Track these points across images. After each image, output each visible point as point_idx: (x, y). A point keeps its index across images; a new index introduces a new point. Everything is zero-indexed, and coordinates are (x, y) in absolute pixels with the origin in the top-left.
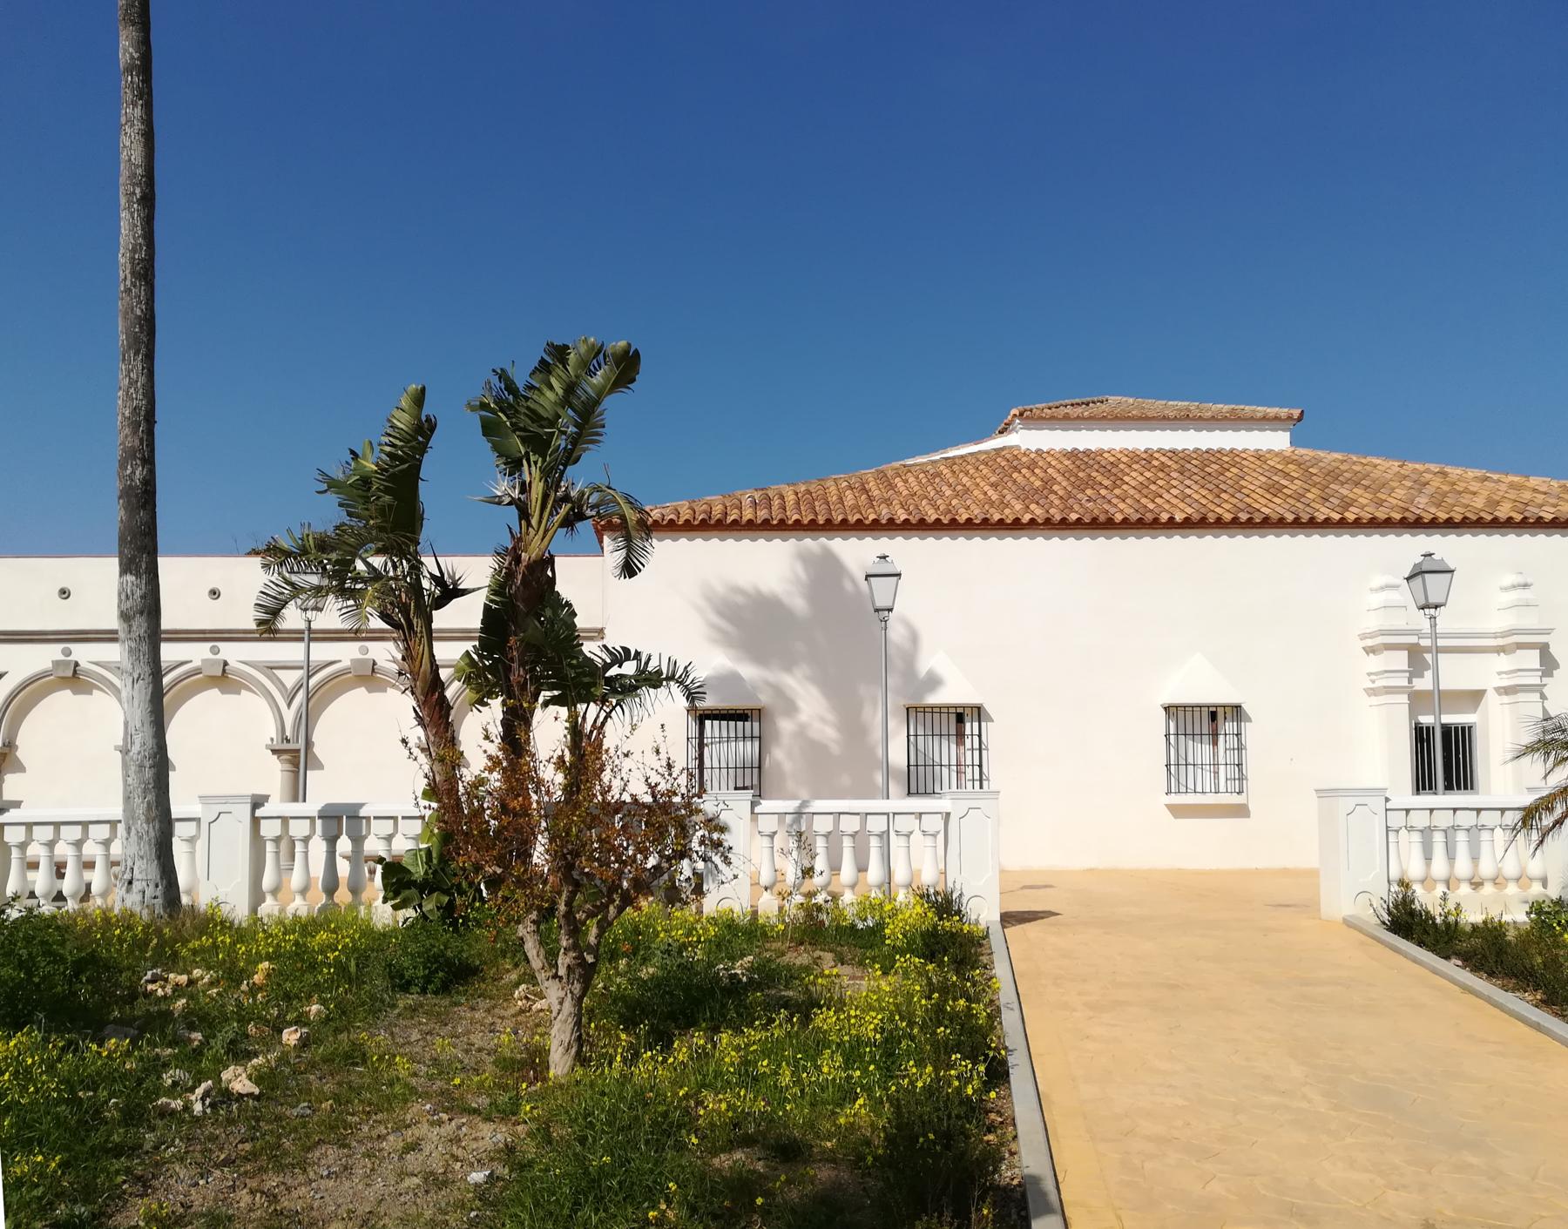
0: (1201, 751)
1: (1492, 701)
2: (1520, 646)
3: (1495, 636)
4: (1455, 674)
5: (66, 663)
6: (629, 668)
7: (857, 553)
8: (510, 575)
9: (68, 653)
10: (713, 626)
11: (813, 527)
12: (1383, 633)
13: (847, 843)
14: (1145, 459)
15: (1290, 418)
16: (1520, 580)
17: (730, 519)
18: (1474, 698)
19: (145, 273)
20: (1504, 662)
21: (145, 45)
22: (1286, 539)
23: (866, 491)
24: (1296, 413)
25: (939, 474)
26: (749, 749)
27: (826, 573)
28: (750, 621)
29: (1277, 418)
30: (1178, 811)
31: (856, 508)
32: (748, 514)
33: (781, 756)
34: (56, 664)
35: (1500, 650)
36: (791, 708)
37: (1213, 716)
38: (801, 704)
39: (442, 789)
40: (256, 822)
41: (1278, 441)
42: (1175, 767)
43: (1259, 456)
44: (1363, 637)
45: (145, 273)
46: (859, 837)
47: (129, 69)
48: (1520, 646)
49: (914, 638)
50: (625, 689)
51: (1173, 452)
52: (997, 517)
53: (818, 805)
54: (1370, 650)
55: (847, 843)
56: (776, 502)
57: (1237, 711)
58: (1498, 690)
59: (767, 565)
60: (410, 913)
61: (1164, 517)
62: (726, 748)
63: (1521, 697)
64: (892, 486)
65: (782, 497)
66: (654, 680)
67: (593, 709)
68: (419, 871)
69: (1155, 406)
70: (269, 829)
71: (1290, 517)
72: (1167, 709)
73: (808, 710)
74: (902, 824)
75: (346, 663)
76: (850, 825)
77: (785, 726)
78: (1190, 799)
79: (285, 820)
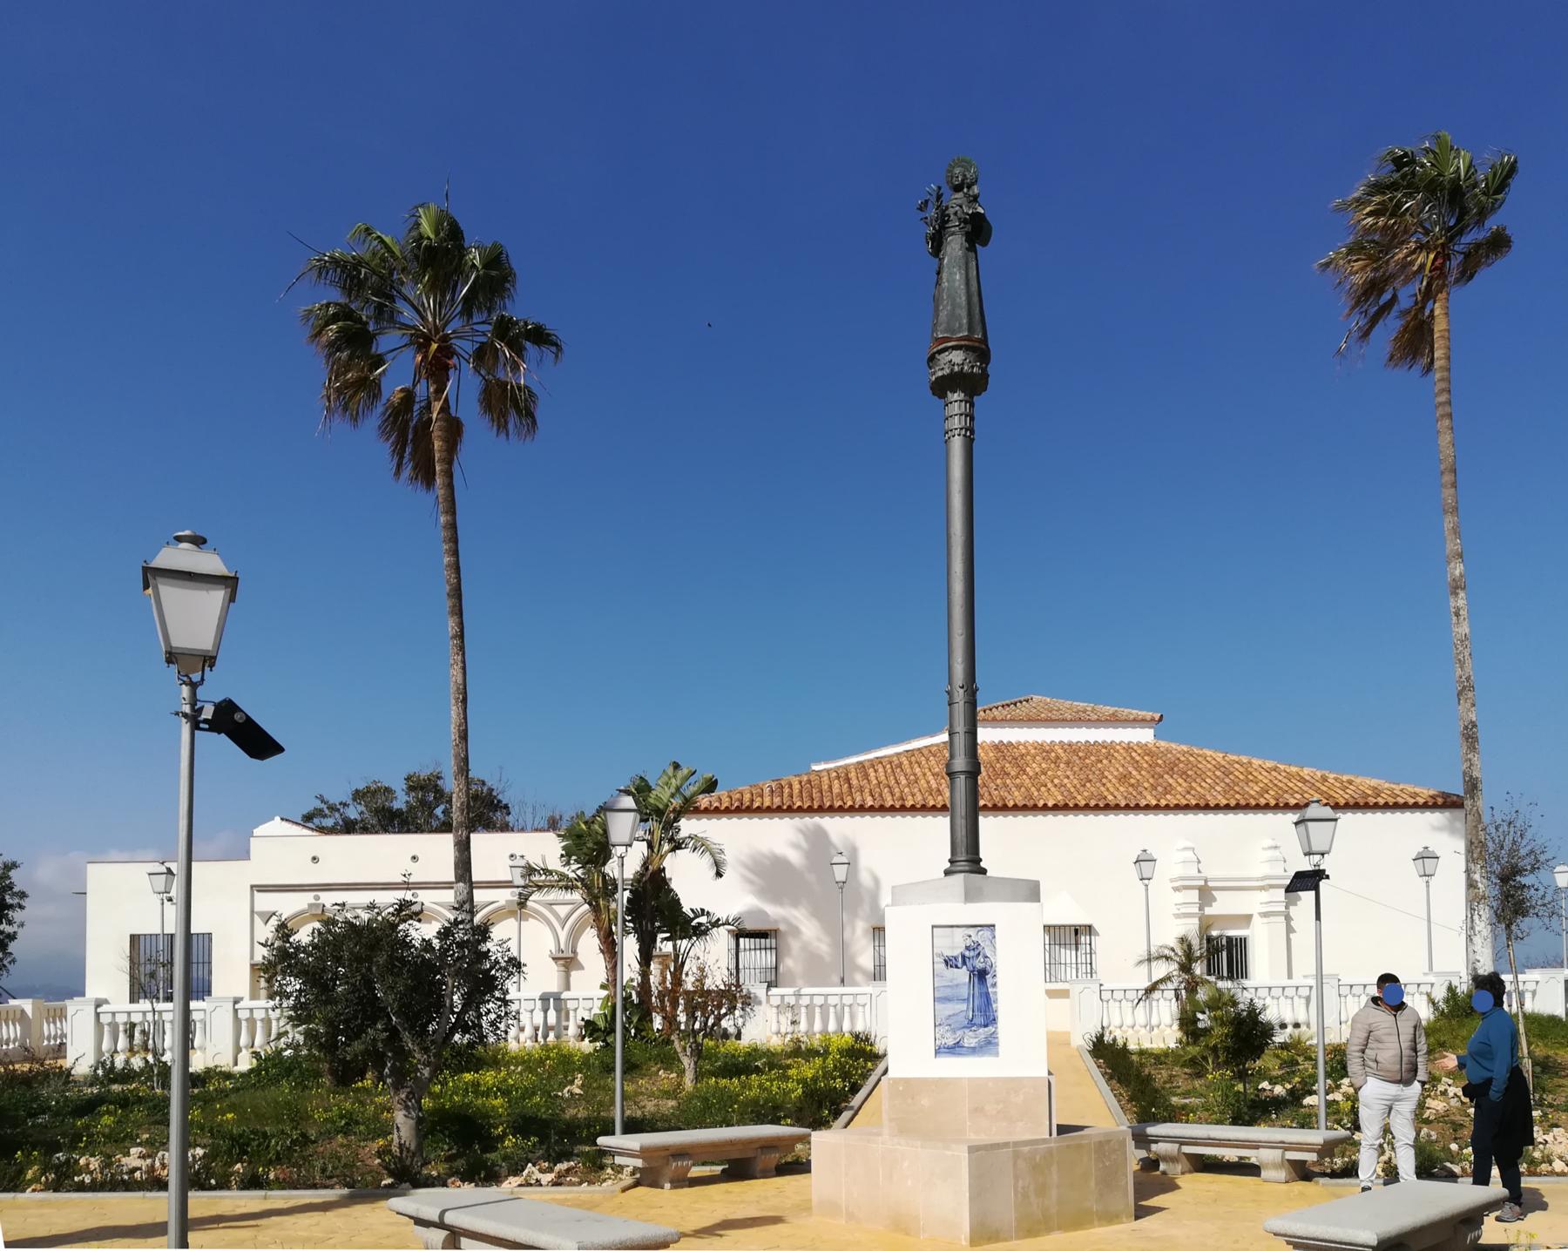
0: (1067, 955)
1: (1256, 920)
2: (1272, 886)
3: (1258, 880)
4: (1223, 905)
5: (317, 905)
6: (703, 920)
7: (837, 827)
8: (642, 875)
9: (317, 898)
10: (743, 876)
11: (810, 810)
12: (1182, 879)
13: (818, 1010)
14: (1044, 750)
15: (1153, 719)
16: (1273, 843)
17: (756, 805)
18: (1247, 919)
19: (464, 736)
20: (1264, 896)
21: (461, 625)
22: (1122, 817)
23: (848, 780)
24: (1157, 716)
25: (900, 765)
26: (768, 959)
27: (819, 841)
28: (771, 875)
29: (1143, 720)
30: (1051, 994)
31: (841, 796)
32: (767, 803)
33: (789, 963)
34: (311, 905)
35: (1262, 888)
36: (796, 931)
37: (1076, 932)
38: (803, 929)
39: (610, 983)
40: (236, 1011)
41: (1145, 735)
42: (1051, 968)
43: (1129, 748)
44: (1172, 881)
45: (464, 736)
46: (824, 1008)
47: (454, 637)
48: (1272, 886)
49: (877, 881)
50: (700, 932)
51: (1070, 745)
52: (932, 803)
53: (805, 991)
54: (1176, 889)
55: (818, 1010)
56: (786, 790)
57: (1089, 929)
58: (1265, 915)
59: (778, 836)
60: (598, 1044)
61: (1041, 804)
62: (756, 958)
63: (1272, 919)
64: (866, 776)
65: (791, 786)
66: (716, 924)
67: (685, 942)
68: (601, 1024)
69: (1066, 706)
70: (243, 1015)
71: (1123, 804)
72: (1047, 928)
73: (806, 929)
74: (861, 1000)
75: (502, 903)
76: (819, 1001)
77: (794, 945)
78: (1060, 986)
79: (251, 1010)
